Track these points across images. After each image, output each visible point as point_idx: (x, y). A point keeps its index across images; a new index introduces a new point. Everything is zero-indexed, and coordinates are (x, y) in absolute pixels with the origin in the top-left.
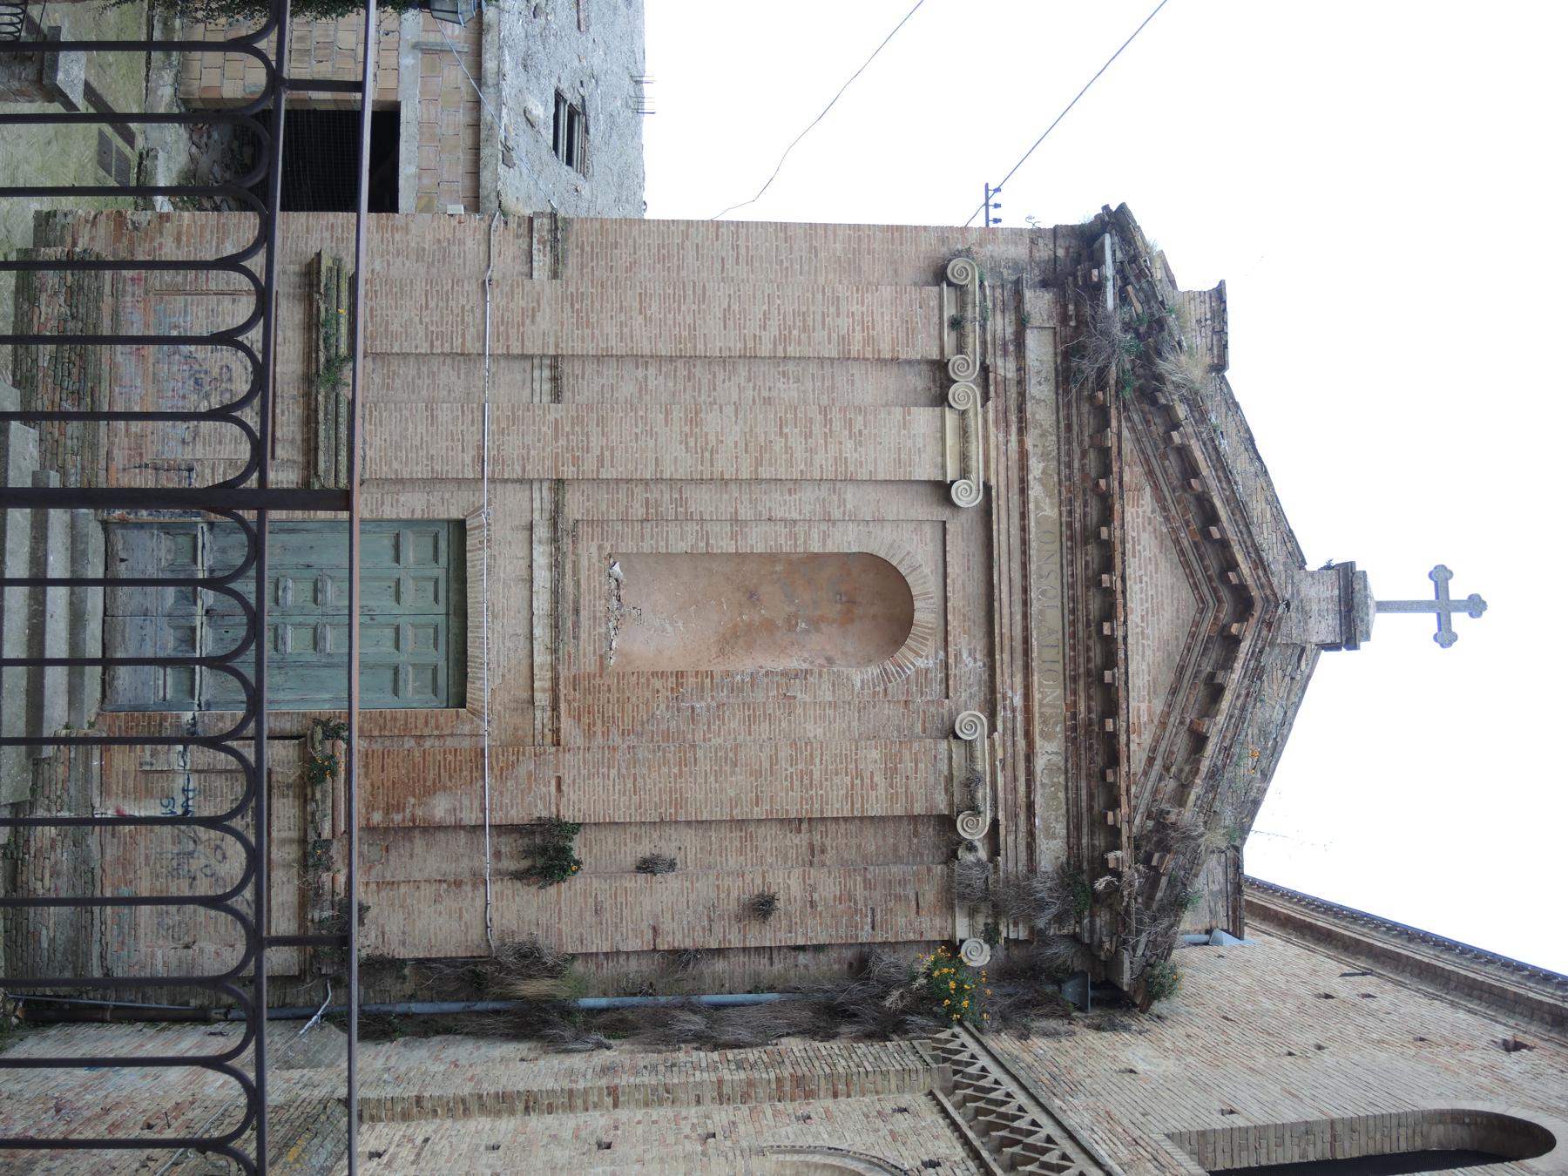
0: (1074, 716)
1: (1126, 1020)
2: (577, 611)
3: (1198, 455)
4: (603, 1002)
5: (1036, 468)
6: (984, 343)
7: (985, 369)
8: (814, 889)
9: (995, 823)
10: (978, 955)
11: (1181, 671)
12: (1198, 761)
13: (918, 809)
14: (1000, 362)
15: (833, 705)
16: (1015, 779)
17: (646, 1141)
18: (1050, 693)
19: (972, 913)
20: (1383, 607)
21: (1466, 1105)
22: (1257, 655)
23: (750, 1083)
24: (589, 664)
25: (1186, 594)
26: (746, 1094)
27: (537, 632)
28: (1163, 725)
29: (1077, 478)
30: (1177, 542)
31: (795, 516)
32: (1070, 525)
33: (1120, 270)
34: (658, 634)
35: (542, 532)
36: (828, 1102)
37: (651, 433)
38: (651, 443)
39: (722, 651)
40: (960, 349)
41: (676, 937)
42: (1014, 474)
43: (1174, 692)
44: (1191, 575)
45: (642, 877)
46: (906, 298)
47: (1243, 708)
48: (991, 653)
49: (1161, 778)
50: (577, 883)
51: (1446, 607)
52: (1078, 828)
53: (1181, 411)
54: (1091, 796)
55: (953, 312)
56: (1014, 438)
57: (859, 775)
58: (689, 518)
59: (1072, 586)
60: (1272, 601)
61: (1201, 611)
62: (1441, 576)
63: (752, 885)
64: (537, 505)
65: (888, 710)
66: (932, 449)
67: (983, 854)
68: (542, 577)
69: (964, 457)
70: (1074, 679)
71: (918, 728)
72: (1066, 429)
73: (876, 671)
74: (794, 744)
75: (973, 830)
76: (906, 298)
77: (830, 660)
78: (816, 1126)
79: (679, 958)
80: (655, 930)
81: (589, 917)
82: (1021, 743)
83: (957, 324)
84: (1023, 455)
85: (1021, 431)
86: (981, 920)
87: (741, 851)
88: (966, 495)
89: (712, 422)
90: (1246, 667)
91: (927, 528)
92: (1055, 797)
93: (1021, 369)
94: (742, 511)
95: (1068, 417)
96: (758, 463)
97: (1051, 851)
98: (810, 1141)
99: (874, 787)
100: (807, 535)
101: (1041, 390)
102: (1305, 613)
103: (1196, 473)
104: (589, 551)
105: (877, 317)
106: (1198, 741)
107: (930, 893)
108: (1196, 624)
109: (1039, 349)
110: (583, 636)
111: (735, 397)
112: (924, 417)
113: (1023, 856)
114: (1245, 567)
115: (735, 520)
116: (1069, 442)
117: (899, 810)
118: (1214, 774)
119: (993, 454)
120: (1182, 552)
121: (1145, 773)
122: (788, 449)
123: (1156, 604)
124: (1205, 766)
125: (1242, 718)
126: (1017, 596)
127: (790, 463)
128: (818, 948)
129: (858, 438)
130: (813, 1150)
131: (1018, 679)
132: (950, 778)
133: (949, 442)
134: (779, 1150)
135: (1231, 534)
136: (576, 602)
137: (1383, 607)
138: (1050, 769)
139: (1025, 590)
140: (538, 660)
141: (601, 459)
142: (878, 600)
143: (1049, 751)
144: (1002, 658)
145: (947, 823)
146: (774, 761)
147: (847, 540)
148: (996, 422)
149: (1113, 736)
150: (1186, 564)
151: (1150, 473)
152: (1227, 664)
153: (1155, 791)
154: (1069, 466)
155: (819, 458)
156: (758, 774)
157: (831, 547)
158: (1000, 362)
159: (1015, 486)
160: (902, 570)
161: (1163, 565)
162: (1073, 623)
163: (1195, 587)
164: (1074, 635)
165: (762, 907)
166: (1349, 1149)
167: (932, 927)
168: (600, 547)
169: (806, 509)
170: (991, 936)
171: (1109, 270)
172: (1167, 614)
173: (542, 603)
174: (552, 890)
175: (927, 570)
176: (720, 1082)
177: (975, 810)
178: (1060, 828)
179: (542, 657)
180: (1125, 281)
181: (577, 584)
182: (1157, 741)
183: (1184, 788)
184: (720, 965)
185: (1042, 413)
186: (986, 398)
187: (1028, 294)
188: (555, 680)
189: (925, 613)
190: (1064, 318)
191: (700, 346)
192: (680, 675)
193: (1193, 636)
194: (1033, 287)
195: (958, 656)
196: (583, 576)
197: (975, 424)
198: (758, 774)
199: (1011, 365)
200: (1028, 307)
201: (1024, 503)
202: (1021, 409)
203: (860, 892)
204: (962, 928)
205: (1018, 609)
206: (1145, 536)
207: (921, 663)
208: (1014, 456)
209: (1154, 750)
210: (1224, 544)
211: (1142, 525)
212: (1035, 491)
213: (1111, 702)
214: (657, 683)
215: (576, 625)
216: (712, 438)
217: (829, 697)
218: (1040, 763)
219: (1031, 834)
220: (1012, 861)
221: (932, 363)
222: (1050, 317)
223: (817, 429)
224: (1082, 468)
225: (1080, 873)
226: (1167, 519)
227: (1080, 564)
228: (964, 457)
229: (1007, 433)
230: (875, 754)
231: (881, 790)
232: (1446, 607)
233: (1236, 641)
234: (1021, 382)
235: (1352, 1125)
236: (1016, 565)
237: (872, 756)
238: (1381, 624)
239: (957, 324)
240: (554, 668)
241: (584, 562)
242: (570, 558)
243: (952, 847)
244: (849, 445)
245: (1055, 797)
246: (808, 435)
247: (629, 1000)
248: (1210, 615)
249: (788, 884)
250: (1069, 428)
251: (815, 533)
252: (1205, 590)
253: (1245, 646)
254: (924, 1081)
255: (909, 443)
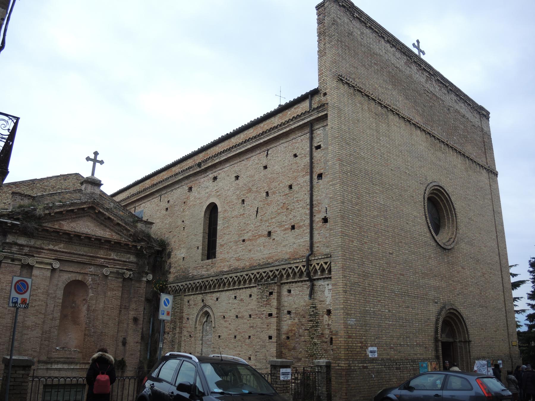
0: (107, 249)
1: (168, 251)
2: (68, 358)
3: (58, 210)
4: (148, 354)
5: (51, 247)
6: (19, 254)
7: (26, 255)
8: (133, 309)
9: (126, 269)
10: (150, 277)
11: (102, 224)
12: (122, 226)
13: (121, 285)
14: (24, 251)
15: (96, 301)
16: (118, 263)
17: (190, 347)
18: (101, 253)
19: (143, 277)
20: (93, 174)
21: (204, 210)
22: (104, 209)
23: (179, 327)
24: (80, 355)
25: (85, 219)
26: (181, 328)
27: (72, 367)
28: (112, 230)
29: (56, 238)
30: (74, 218)
31: (53, 305)
32: (66, 242)
33: (9, 219)
34: (73, 339)
35: (49, 366)
36: (184, 314)
37: (30, 338)
38: (32, 339)
39: (78, 324)
40: (20, 260)
41: (138, 339)
42: (52, 252)
43: (106, 226)
44: (82, 217)
45: (127, 345)
46: (4, 271)
47: (114, 214)
48: (91, 264)
49: (123, 233)
50: (126, 359)
51: (95, 160)
52: (129, 252)
53: (47, 212)
54: (125, 249)
55: (10, 260)
56: (44, 251)
57: (113, 297)
58: (50, 331)
59: (80, 244)
60: (93, 203)
61: (90, 216)
62: (88, 159)
63: (131, 322)
64: (42, 367)
65: (99, 289)
66: (43, 271)
67: (131, 273)
68: (60, 366)
69: (47, 264)
70: (100, 247)
71: (104, 282)
72: (43, 238)
73: (90, 290)
74: (104, 311)
75: (128, 274)
76: (4, 271)
77: (84, 300)
78: (191, 317)
79: (142, 338)
80: (137, 343)
81: (133, 356)
82: (111, 261)
83: (13, 260)
84: (49, 250)
85: (43, 249)
86: (144, 275)
87: (123, 323)
88: (57, 265)
89: (29, 323)
90: (106, 211)
91: (61, 274)
92: (122, 256)
93: (27, 247)
94: (50, 318)
95: (41, 237)
96: (40, 313)
97: (133, 258)
98: (194, 319)
99: (115, 294)
100: (58, 303)
101: (32, 242)
102: (93, 193)
103: (62, 212)
104: (54, 355)
105: (8, 279)
106: (118, 224)
107: (137, 285)
108: (92, 218)
109: (22, 241)
110: (74, 357)
111: (22, 317)
112: (35, 272)
113: (133, 264)
114: (85, 206)
115: (52, 320)
116: (47, 238)
117: (121, 289)
118: (126, 223)
119: (46, 257)
120: (76, 218)
121: (121, 236)
122: (38, 306)
123: (86, 227)
124: (124, 225)
125: (116, 215)
126: (81, 257)
127: (42, 305)
128: (144, 309)
129: (38, 288)
130: (196, 319)
131: (98, 259)
132: (116, 277)
133: (42, 267)
134: (195, 325)
135: (78, 207)
136: (66, 358)
137: (93, 174)
138: (117, 256)
139: (80, 255)
140: (78, 367)
141: (34, 351)
142: (74, 288)
143: (113, 256)
144: (93, 262)
145: (124, 279)
146: (107, 315)
147: (60, 293)
148: (39, 255)
149: (115, 242)
150: (79, 217)
151: (57, 221)
152: (103, 215)
153: (125, 235)
154: (52, 239)
155: (41, 298)
156: (110, 319)
157: (61, 297)
158: (24, 251)
159: (56, 253)
160: (69, 281)
161: (78, 222)
162: (88, 245)
163: (84, 216)
164: (91, 246)
165: (135, 320)
166: (207, 231)
167: (143, 285)
168: (54, 352)
169: (52, 302)
170: (147, 274)
171: (10, 221)
172: (89, 224)
173: (66, 366)
174: (127, 364)
175: (70, 276)
176: (179, 333)
177: (124, 273)
178: (129, 256)
179: (78, 367)
180: (13, 218)
181: (62, 358)
182: (115, 232)
183: (126, 229)
184: (144, 329)
185: (39, 243)
186: (33, 256)
187: (7, 241)
188: (83, 363)
189: (80, 278)
190: (16, 233)
191: (9, 325)
192: (85, 335)
193: (95, 219)
194: (5, 240)
195: (90, 272)
196: (60, 356)
197: (40, 260)
198: (110, 319)
199: (26, 248)
200: (11, 241)
201: (60, 251)
202: (37, 248)
203: (135, 299)
204: (145, 279)
205: (83, 257)
206: (71, 225)
207: (90, 280)
208: (48, 252)
209: (117, 233)
210: (78, 209)
211: (68, 226)
212: (56, 248)
213: (108, 241)
214: (86, 340)
215: (71, 358)
216: (33, 324)
217: (94, 301)
218: (116, 258)
219: (129, 262)
220: (133, 267)
221: (22, 267)
222: (14, 236)
223: (34, 298)
224: (54, 237)
225: (139, 254)
226: (68, 219)
227: (76, 241)
228: (47, 264)
229: (42, 252)
230: (109, 293)
231: (116, 292)
232: (95, 160)
233: (99, 212)
234: (31, 247)
235: (204, 230)
236: (74, 256)
237: (109, 293)
238: (97, 176)
239: (13, 260)
240: (81, 364)
241: (57, 356)
242: (56, 359)
243: (130, 279)
244: (39, 291)
245: (122, 256)
246: (36, 300)
247: (149, 349)
248: (91, 215)
249: (132, 314)
250: (44, 237)
251: (58, 301)
252: (85, 214)
253: (101, 210)
254: (183, 296)
255: (41, 276)
